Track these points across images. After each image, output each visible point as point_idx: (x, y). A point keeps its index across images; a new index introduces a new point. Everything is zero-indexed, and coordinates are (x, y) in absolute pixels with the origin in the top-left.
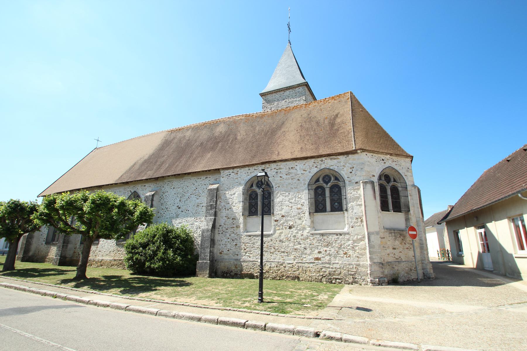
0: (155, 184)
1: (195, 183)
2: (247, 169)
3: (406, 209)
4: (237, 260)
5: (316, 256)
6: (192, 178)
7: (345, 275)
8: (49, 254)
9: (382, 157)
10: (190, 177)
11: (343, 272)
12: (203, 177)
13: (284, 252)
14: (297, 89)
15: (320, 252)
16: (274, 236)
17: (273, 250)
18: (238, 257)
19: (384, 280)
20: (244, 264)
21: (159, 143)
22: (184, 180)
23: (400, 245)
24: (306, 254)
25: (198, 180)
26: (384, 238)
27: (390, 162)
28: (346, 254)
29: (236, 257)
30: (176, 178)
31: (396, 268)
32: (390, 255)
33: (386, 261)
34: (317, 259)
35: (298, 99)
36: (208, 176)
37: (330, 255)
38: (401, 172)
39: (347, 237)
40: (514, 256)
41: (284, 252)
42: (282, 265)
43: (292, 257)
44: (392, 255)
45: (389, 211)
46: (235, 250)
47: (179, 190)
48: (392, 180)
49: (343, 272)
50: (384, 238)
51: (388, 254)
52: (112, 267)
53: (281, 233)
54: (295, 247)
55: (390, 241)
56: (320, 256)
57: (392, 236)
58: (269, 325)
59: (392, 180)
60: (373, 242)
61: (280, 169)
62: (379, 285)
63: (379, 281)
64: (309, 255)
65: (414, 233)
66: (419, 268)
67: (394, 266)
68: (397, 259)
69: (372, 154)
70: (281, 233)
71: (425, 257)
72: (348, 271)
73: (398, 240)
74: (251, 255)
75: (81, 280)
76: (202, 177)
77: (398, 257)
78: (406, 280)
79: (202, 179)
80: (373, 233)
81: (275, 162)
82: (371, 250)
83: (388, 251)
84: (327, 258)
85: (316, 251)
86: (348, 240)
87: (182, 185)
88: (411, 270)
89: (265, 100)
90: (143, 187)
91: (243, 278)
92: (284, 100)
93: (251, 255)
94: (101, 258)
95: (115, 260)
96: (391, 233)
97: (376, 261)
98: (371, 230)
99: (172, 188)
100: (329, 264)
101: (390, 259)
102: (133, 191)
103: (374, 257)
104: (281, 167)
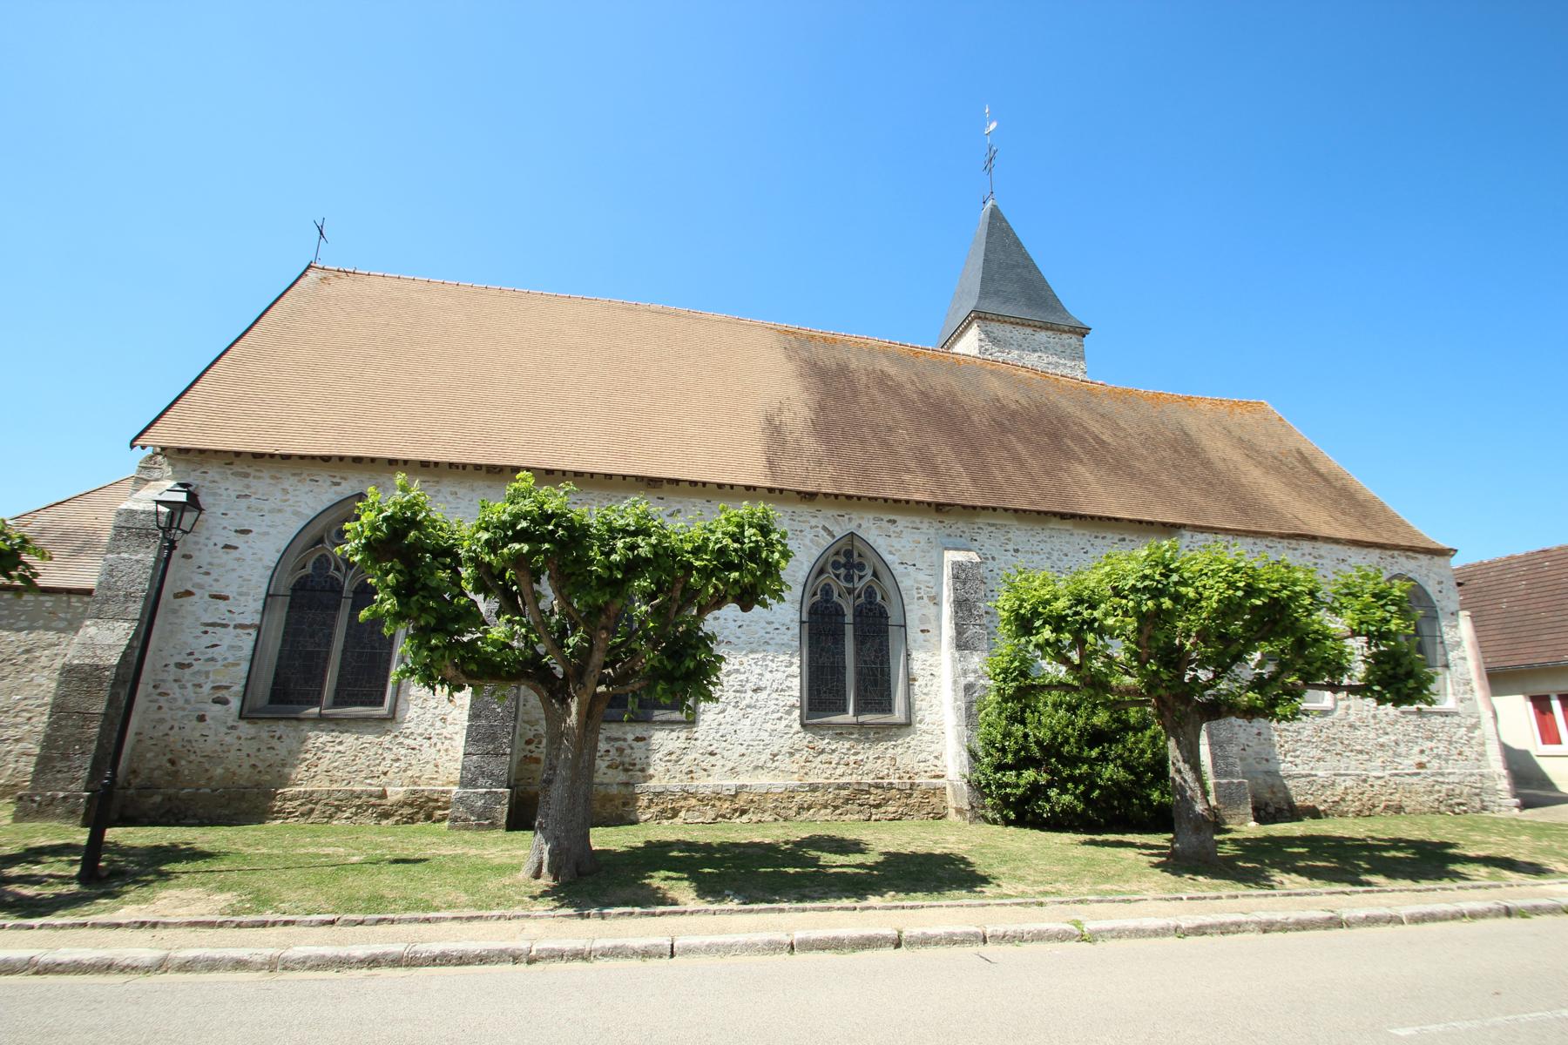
0: (936, 525)
1: (1088, 547)
2: (1250, 540)
4: (1267, 773)
5: (1417, 760)
6: (1076, 532)
7: (1469, 796)
8: (300, 772)
10: (1068, 525)
11: (1466, 790)
12: (1112, 537)
13: (1361, 752)
14: (1065, 336)
15: (1422, 752)
16: (1336, 714)
17: (1339, 747)
18: (1271, 766)
20: (1290, 783)
22: (1047, 532)
24: (1399, 756)
25: (1098, 542)
28: (1460, 754)
29: (1264, 766)
30: (1020, 519)
34: (1421, 765)
35: (1069, 363)
36: (1128, 537)
37: (1438, 756)
39: (1456, 720)
40: (1533, 753)
41: (1361, 752)
42: (1365, 781)
43: (1378, 762)
46: (1257, 748)
47: (1036, 558)
49: (1466, 790)
52: (805, 815)
53: (1348, 707)
54: (1381, 740)
56: (1424, 759)
58: (786, 955)
61: (1321, 557)
64: (1406, 756)
70: (1348, 707)
74: (1298, 761)
75: (588, 882)
76: (1109, 535)
79: (1107, 541)
81: (1314, 538)
84: (1435, 763)
85: (1416, 749)
86: (1459, 726)
87: (1047, 547)
89: (987, 333)
90: (885, 524)
91: (1300, 820)
92: (1035, 351)
93: (1298, 761)
94: (731, 783)
95: (814, 788)
99: (1010, 547)
100: (1442, 775)
102: (839, 533)
104: (1322, 552)
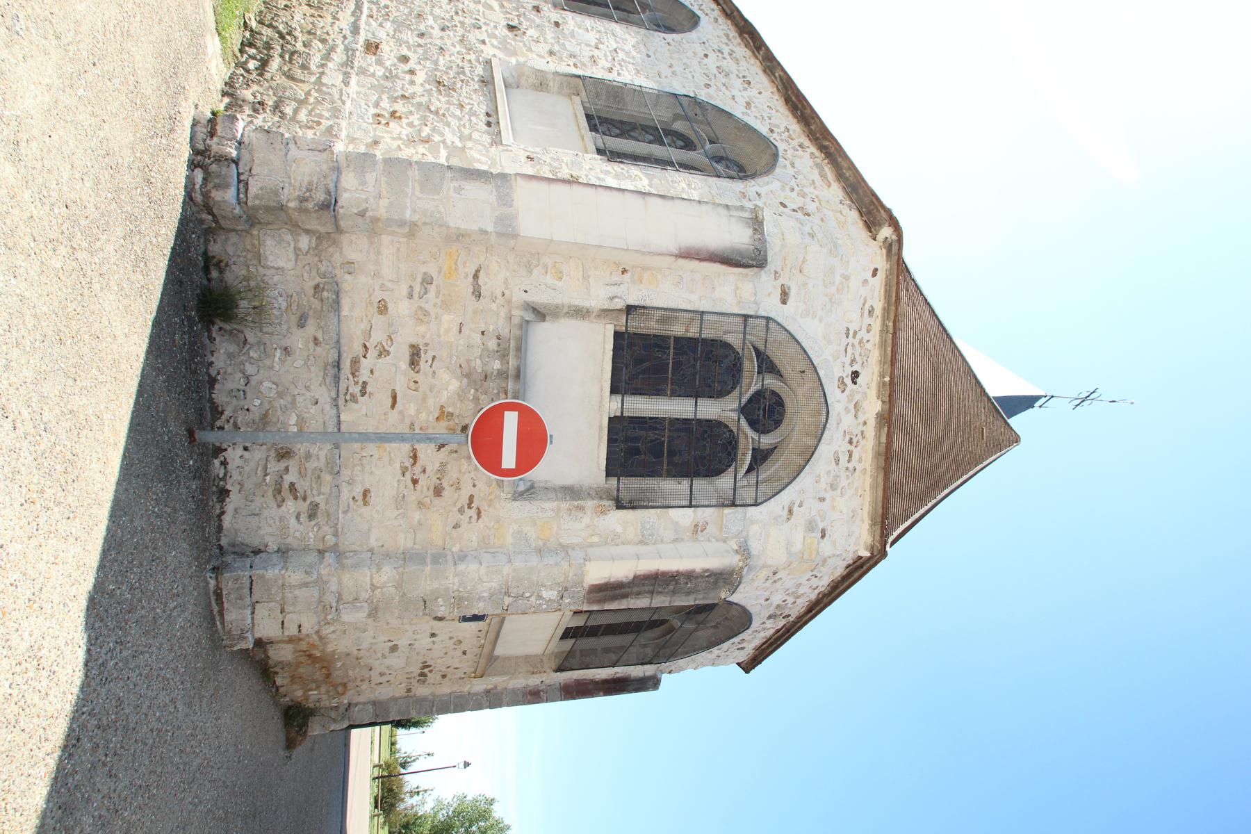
3: (625, 496)
9: (871, 374)
19: (224, 186)
21: (738, 246)
23: (433, 404)
26: (478, 294)
27: (848, 421)
31: (299, 340)
32: (378, 321)
33: (347, 282)
38: (805, 480)
44: (378, 337)
45: (614, 390)
48: (766, 441)
50: (478, 294)
51: (383, 308)
55: (459, 333)
57: (486, 351)
59: (766, 441)
60: (459, 190)
62: (196, 152)
63: (222, 159)
65: (509, 459)
66: (300, 531)
67: (311, 329)
68: (355, 362)
69: (879, 306)
71: (356, 566)
72: (289, 34)
73: (461, 395)
77: (364, 375)
78: (220, 396)
80: (505, 200)
82: (414, 173)
83: (402, 308)
88: (284, 455)
96: (503, 355)
97: (349, 180)
98: (524, 194)
101: (356, 315)
103: (370, 177)
